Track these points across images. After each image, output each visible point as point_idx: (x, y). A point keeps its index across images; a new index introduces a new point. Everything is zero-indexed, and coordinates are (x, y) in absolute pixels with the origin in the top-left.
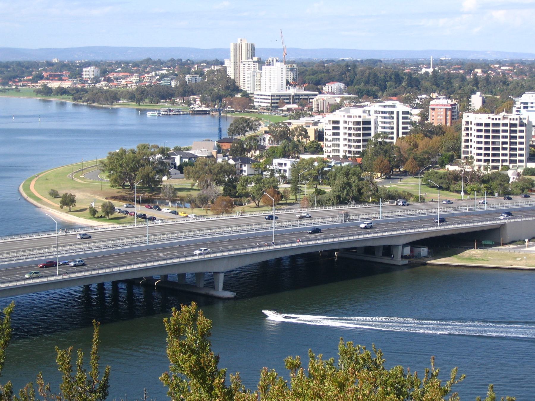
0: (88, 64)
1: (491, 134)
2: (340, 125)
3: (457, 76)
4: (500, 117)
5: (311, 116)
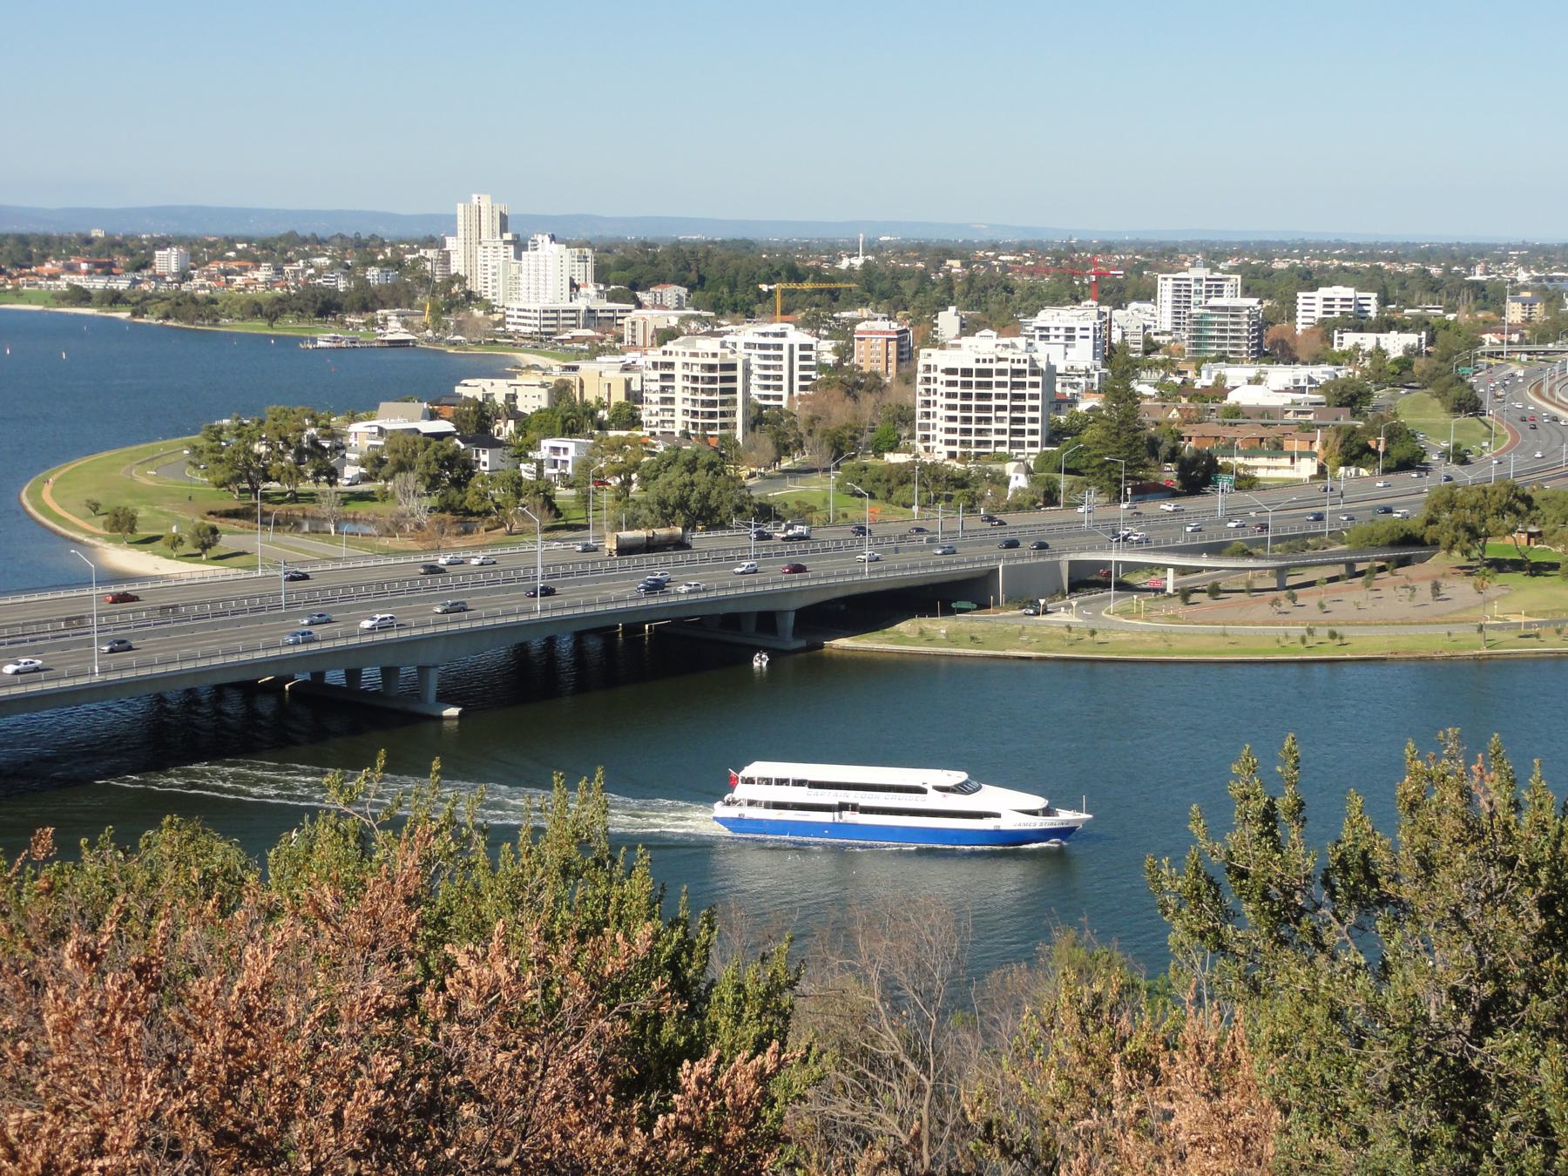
1: (973, 414)
2: (667, 369)
3: (909, 274)
5: (614, 352)
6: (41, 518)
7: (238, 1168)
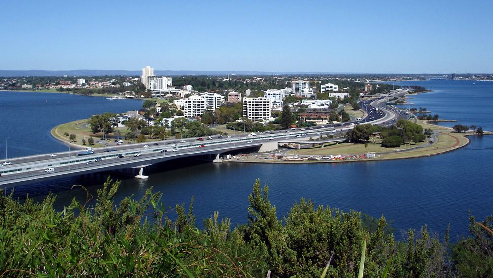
0: (80, 78)
1: (255, 106)
2: (191, 102)
4: (259, 99)
6: (56, 137)
7: (113, 277)
